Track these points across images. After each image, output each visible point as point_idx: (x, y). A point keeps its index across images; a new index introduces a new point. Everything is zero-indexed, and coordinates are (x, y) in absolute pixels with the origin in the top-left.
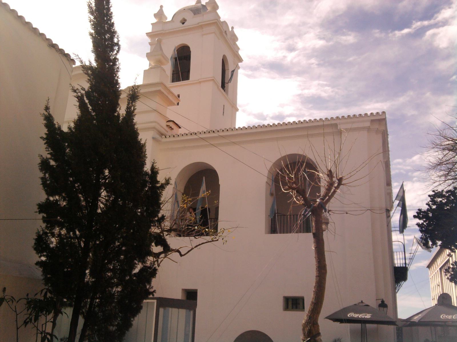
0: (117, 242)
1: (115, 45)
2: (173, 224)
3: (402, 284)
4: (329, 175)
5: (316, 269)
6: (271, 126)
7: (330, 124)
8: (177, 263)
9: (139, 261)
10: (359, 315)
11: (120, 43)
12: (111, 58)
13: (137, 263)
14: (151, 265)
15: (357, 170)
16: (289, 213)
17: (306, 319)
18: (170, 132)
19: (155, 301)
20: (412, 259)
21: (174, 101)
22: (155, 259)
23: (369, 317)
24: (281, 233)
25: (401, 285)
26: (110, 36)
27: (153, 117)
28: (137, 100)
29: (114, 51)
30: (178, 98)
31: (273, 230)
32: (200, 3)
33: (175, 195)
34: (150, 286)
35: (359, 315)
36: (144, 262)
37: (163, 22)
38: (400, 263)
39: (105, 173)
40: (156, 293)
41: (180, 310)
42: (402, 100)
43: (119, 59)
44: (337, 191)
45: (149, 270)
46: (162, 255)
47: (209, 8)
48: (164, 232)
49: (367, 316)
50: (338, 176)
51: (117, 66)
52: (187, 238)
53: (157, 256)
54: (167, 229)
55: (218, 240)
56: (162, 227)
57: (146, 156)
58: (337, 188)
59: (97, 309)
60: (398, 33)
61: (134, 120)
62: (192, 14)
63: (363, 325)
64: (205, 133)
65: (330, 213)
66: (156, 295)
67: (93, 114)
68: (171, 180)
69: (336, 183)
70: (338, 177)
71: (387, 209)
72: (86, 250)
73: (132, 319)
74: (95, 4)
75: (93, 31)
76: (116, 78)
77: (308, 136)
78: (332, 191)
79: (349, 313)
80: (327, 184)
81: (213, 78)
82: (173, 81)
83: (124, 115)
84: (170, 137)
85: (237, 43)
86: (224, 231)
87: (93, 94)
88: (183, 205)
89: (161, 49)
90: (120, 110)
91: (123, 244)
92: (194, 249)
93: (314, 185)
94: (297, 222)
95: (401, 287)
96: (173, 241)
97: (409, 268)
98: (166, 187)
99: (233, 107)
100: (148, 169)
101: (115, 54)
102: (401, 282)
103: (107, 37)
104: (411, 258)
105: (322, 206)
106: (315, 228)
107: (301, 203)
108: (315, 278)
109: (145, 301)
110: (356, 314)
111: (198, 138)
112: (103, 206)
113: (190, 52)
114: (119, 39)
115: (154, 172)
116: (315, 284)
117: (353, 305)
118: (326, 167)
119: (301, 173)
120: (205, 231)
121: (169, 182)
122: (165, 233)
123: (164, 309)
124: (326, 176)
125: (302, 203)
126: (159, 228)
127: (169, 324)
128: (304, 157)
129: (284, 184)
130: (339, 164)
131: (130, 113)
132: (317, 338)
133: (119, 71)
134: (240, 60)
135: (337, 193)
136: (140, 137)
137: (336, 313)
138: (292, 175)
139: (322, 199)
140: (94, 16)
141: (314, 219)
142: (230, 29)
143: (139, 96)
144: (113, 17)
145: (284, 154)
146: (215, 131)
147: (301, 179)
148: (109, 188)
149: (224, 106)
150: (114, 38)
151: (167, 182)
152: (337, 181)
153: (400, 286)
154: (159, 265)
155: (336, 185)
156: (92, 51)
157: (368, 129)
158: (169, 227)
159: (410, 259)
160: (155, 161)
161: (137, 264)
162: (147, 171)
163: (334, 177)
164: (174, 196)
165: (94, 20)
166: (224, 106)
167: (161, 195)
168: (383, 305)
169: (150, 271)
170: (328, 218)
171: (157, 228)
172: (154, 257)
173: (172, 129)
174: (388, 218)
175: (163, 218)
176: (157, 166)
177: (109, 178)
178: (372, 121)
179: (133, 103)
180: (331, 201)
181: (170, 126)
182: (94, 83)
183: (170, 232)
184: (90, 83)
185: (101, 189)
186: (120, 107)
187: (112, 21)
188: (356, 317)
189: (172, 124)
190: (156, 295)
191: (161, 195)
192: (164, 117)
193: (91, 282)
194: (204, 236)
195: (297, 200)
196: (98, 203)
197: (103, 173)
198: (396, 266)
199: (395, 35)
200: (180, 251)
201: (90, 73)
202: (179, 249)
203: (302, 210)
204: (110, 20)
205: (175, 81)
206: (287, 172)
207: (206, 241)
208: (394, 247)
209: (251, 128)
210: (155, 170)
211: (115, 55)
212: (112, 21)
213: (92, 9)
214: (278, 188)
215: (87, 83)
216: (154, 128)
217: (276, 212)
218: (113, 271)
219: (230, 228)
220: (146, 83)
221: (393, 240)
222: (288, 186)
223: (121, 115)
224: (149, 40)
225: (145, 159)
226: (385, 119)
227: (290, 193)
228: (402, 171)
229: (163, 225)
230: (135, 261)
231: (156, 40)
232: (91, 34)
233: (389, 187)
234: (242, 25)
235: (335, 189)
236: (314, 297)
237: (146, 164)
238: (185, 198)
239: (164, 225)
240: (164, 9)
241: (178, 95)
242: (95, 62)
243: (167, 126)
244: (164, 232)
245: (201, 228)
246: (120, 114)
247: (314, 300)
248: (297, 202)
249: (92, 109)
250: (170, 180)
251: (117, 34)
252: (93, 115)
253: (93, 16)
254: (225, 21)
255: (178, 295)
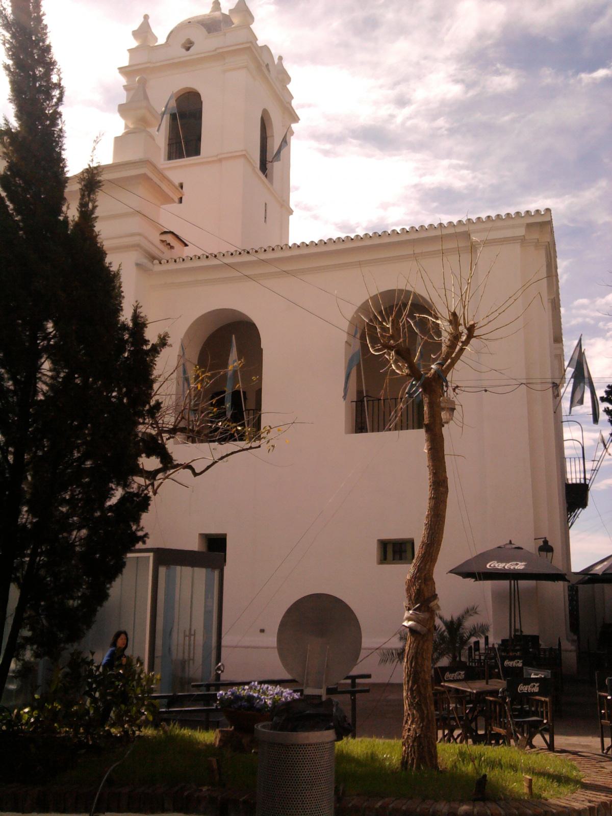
0: (75, 452)
1: (53, 86)
2: (179, 418)
3: (578, 512)
4: (453, 322)
5: (430, 486)
6: (352, 239)
7: (453, 233)
8: (188, 487)
9: (118, 484)
10: (504, 564)
11: (63, 84)
12: (47, 112)
13: (114, 487)
14: (139, 490)
15: (499, 311)
16: (383, 391)
17: (412, 571)
18: (167, 254)
19: (151, 555)
20: (596, 471)
21: (171, 194)
22: (148, 482)
23: (522, 567)
24: (373, 432)
25: (577, 514)
26: (43, 71)
27: (133, 225)
28: (97, 190)
29: (53, 99)
30: (180, 189)
31: (360, 427)
32: (218, 11)
33: (182, 366)
34: (138, 526)
35: (506, 565)
36: (126, 485)
37: (149, 46)
38: (579, 477)
39: (47, 329)
40: (148, 538)
41: (196, 569)
42: (589, 195)
43: (63, 114)
44: (465, 348)
45: (135, 498)
46: (160, 476)
47: (236, 20)
48: (163, 435)
49: (518, 566)
50: (466, 322)
51: (60, 127)
52: (206, 445)
53: (151, 475)
54: (168, 428)
55: (259, 447)
56: (160, 425)
57: (122, 294)
58: (466, 343)
59: (42, 572)
60: (585, 77)
61: (95, 226)
62: (204, 31)
63: (512, 582)
64: (232, 254)
65: (457, 391)
66: (150, 543)
67: (16, 219)
68: (169, 337)
69: (463, 334)
70: (467, 325)
71: (554, 383)
72: (19, 468)
73: (108, 586)
74: (12, 10)
75: (10, 62)
76: (57, 150)
77: (415, 257)
78: (458, 348)
79: (488, 563)
80: (448, 337)
81: (244, 153)
82: (171, 156)
83: (77, 219)
84: (168, 262)
85: (289, 87)
86: (271, 430)
87: (15, 181)
88: (195, 385)
89: (146, 97)
90: (69, 210)
91: (85, 457)
92: (218, 463)
93: (426, 340)
94: (396, 406)
95: (577, 519)
96: (179, 449)
97: (591, 486)
98: (161, 350)
99: (282, 206)
100: (126, 319)
101: (54, 103)
102: (577, 510)
103: (37, 72)
104: (594, 469)
105: (440, 378)
106: (427, 415)
107: (405, 374)
108: (428, 501)
109: (129, 555)
110: (500, 564)
111: (222, 264)
112: (47, 388)
113: (200, 103)
114: (61, 76)
115: (139, 324)
116: (428, 512)
117: (496, 548)
118: (448, 307)
119: (404, 318)
120: (237, 430)
121: (166, 341)
122: (165, 436)
123: (167, 569)
124: (447, 324)
125: (406, 372)
126: (154, 428)
127: (177, 590)
128: (408, 293)
129: (374, 341)
130: (469, 301)
131: (87, 217)
132: (432, 604)
133: (63, 137)
134: (296, 119)
135: (465, 352)
136: (108, 260)
137: (467, 563)
138: (387, 324)
139: (441, 365)
140: (11, 32)
141: (426, 400)
142: (276, 61)
143: (100, 182)
144: (48, 34)
145: (374, 292)
146: (250, 252)
147: (404, 329)
148: (55, 354)
149: (266, 204)
150: (52, 75)
151: (163, 342)
152: (466, 331)
153: (576, 516)
154: (155, 493)
155: (464, 338)
156: (9, 99)
157: (522, 240)
158: (171, 425)
159: (592, 470)
160: (138, 304)
161: (113, 490)
162: (125, 323)
163: (461, 325)
164: (181, 369)
165: (11, 41)
166: (266, 204)
167: (152, 364)
168: (546, 548)
169: (138, 500)
170: (454, 401)
171: (150, 427)
172: (147, 478)
173: (172, 247)
174: (556, 398)
175: (158, 405)
176: (143, 312)
177: (54, 337)
178: (529, 226)
179: (91, 196)
180: (456, 366)
181: (168, 242)
182: (15, 159)
183: (175, 434)
184: (7, 160)
185: (41, 357)
186: (69, 205)
187: (47, 43)
188: (499, 568)
189: (172, 238)
190: (150, 543)
191: (152, 364)
192: (153, 222)
193: (31, 523)
194: (235, 440)
195: (400, 370)
196: (36, 383)
197: (44, 329)
198: (570, 482)
199: (580, 81)
200: (193, 466)
201: (6, 140)
202: (190, 462)
203: (407, 385)
204: (44, 41)
205: (174, 157)
206: (378, 318)
207: (239, 449)
208: (567, 453)
209: (316, 244)
210: (140, 321)
211: (53, 106)
212: (47, 43)
213: (7, 19)
214: (364, 347)
215: (2, 159)
216: (137, 246)
217: (365, 395)
218: (71, 502)
219: (281, 424)
220: (119, 160)
221: (565, 439)
222: (381, 343)
223: (71, 218)
224: (123, 80)
225: (121, 301)
226: (550, 223)
227: (386, 356)
228: (587, 320)
229: (160, 422)
230: (110, 484)
231: (137, 79)
232: (7, 68)
233: (558, 345)
234: (300, 59)
235: (463, 346)
236: (426, 533)
237: (122, 310)
238: (198, 372)
239: (163, 421)
240: (150, 21)
241: (179, 184)
242: (16, 121)
243: (163, 241)
244: (163, 435)
245: (228, 426)
246: (68, 217)
247: (426, 539)
248: (397, 371)
249: (14, 209)
250: (167, 339)
251: (57, 66)
252: (16, 220)
253: (10, 34)
254: (265, 46)
255: (193, 544)
